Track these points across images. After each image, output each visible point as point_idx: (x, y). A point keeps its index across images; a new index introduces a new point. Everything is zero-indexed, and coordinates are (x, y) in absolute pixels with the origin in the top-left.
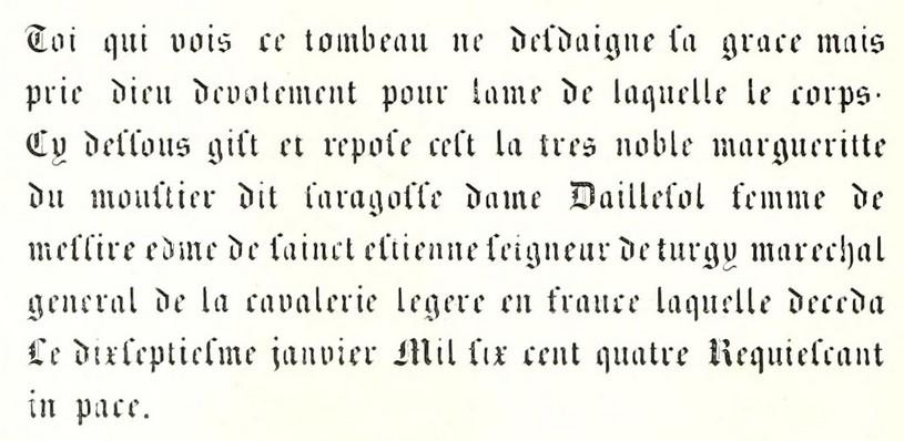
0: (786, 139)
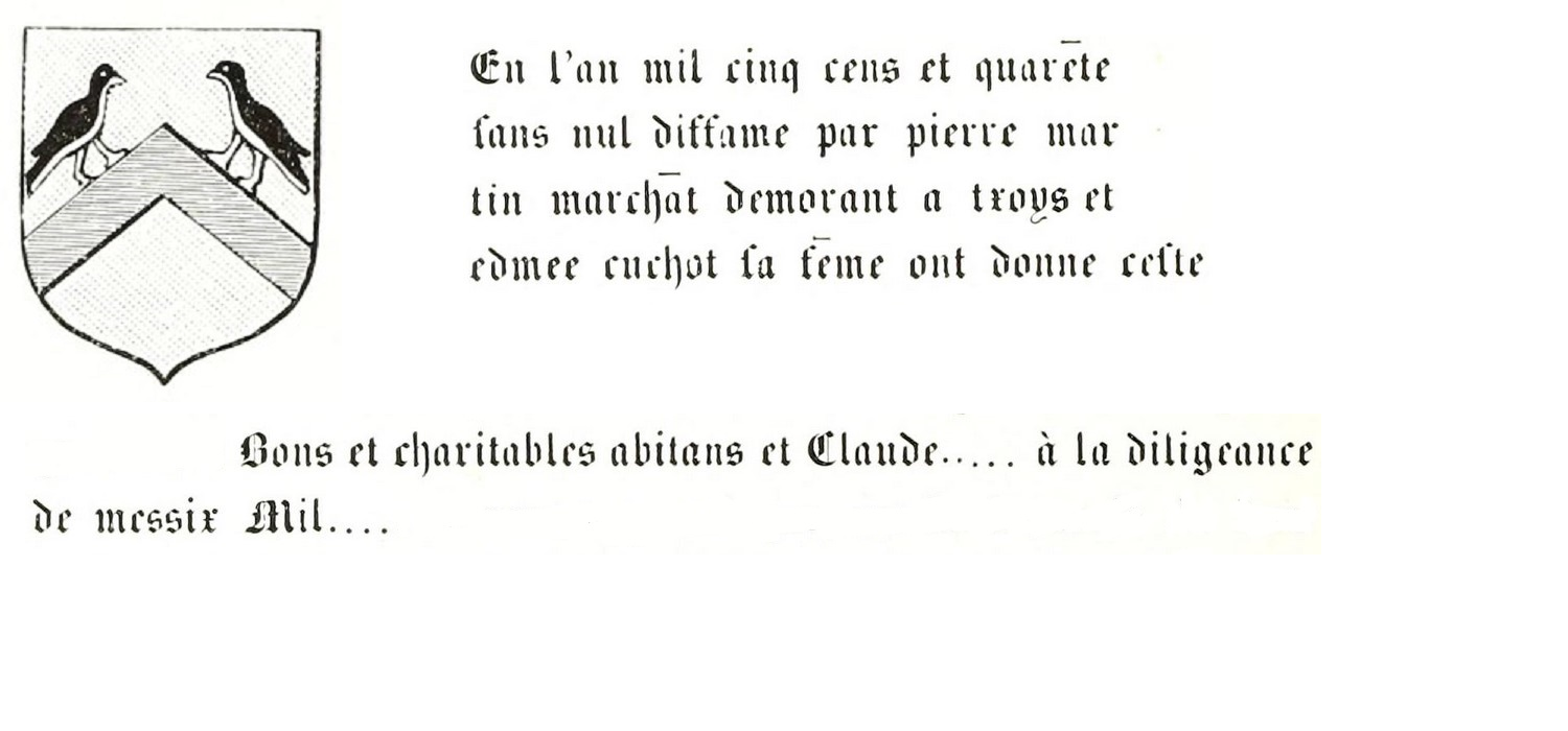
0: (564, 465)
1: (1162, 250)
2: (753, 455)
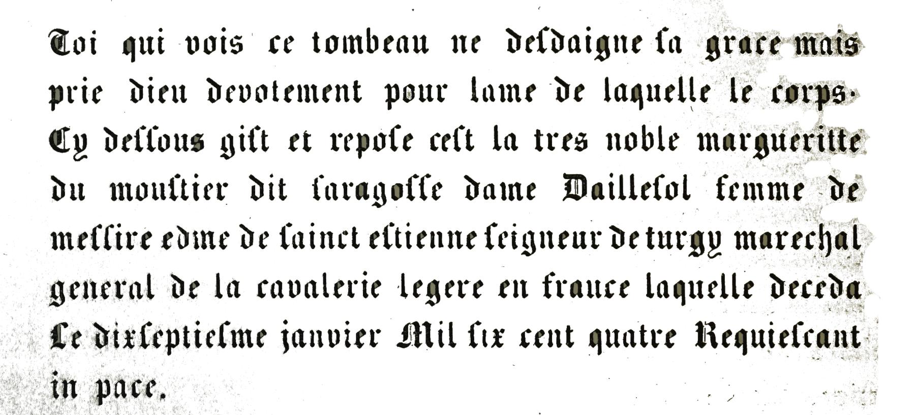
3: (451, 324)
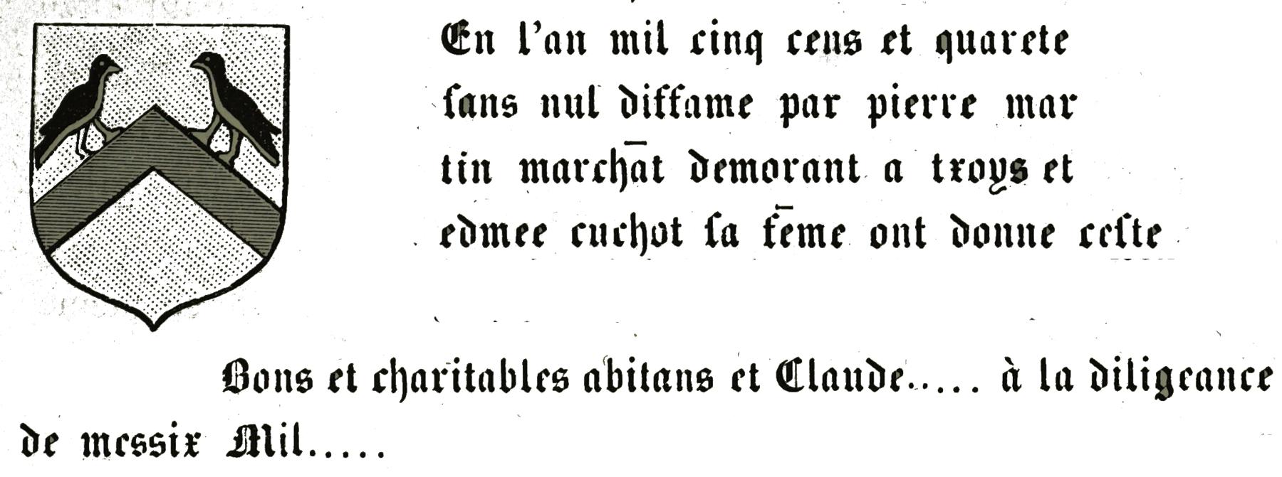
1: (1120, 221)
2: (722, 380)
3: (296, 427)
